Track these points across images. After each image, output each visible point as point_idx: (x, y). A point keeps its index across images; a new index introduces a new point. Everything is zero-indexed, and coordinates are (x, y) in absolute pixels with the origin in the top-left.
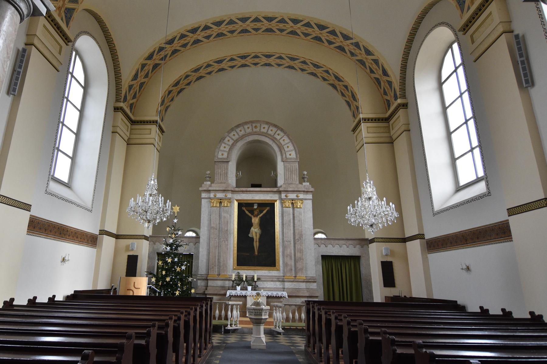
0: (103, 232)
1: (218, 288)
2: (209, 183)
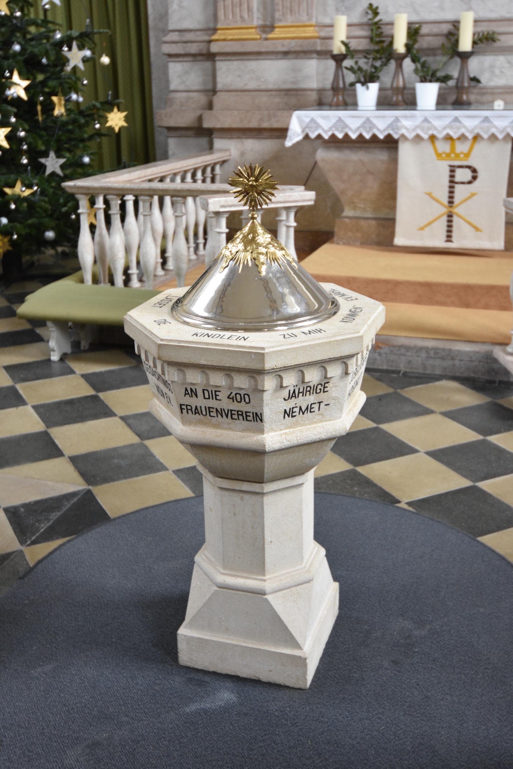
1: (264, 99)
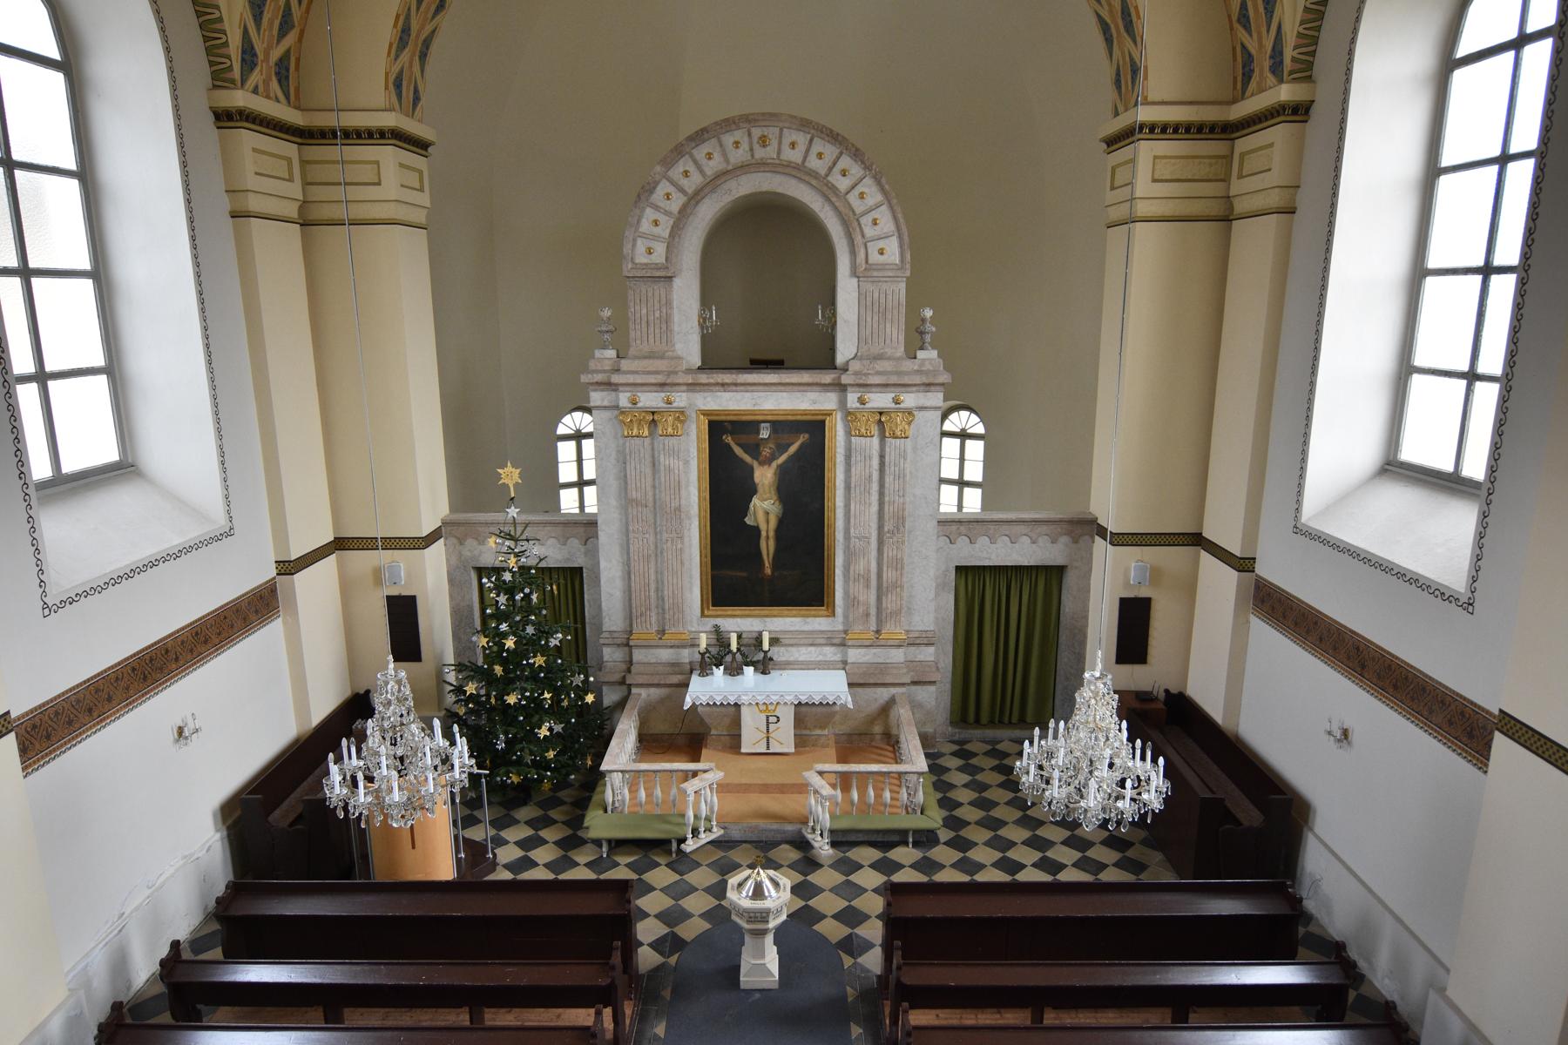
0: (288, 568)
2: (611, 353)
